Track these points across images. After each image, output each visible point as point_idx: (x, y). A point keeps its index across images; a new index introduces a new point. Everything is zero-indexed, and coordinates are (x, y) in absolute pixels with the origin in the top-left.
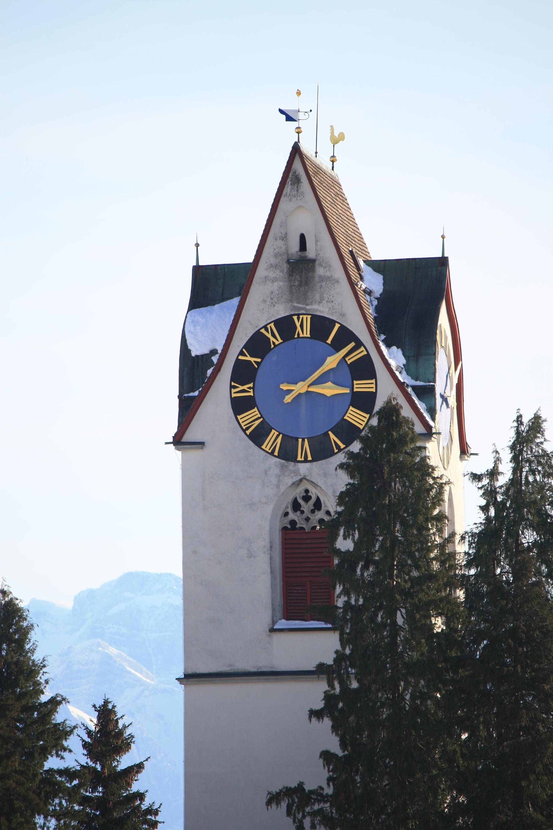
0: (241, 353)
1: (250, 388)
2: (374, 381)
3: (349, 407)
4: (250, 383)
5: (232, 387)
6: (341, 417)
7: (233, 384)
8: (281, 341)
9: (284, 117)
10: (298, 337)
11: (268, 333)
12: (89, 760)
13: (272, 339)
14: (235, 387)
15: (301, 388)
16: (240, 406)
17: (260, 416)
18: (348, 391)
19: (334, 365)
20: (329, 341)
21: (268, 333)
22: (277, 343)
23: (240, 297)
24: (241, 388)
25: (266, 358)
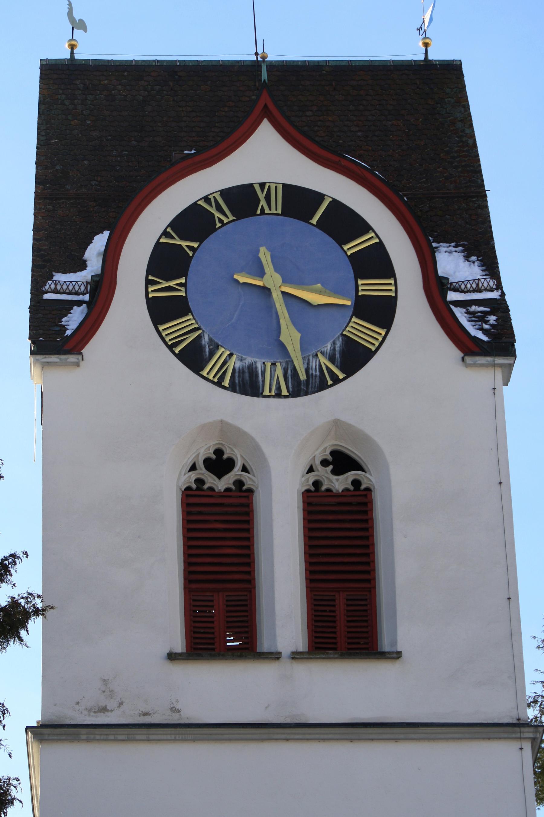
0: (165, 234)
1: (180, 285)
2: (383, 332)
3: (351, 319)
4: (181, 277)
5: (148, 283)
6: (347, 259)
7: (150, 277)
8: (231, 218)
9: (68, 3)
10: (263, 212)
11: (211, 206)
12: (15, 593)
13: (217, 215)
14: (154, 283)
15: (272, 279)
16: (162, 311)
17: (197, 326)
18: (348, 303)
19: (297, 336)
20: (314, 221)
21: (211, 206)
22: (226, 221)
23: (107, 233)
24: (165, 284)
25: (190, 274)
